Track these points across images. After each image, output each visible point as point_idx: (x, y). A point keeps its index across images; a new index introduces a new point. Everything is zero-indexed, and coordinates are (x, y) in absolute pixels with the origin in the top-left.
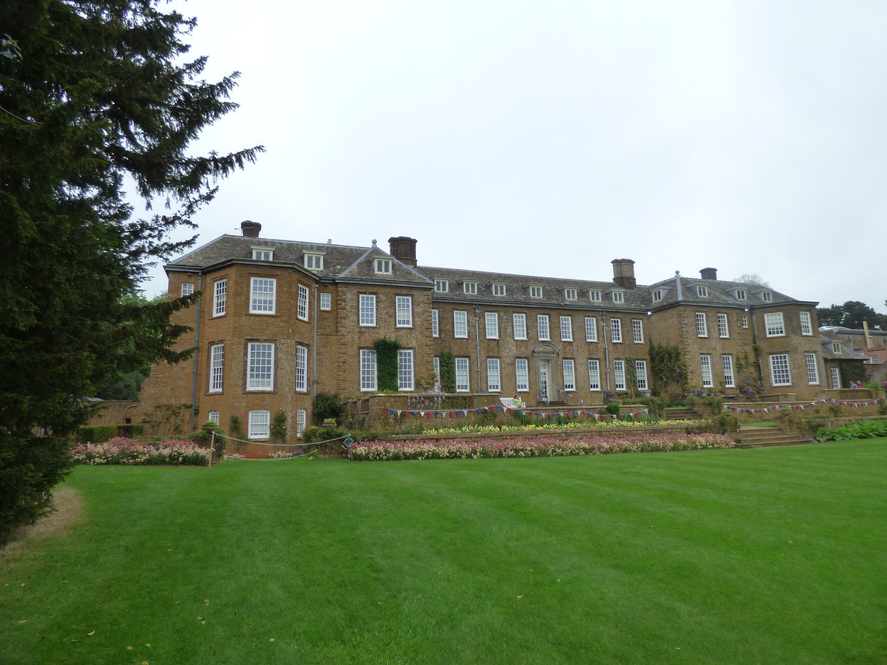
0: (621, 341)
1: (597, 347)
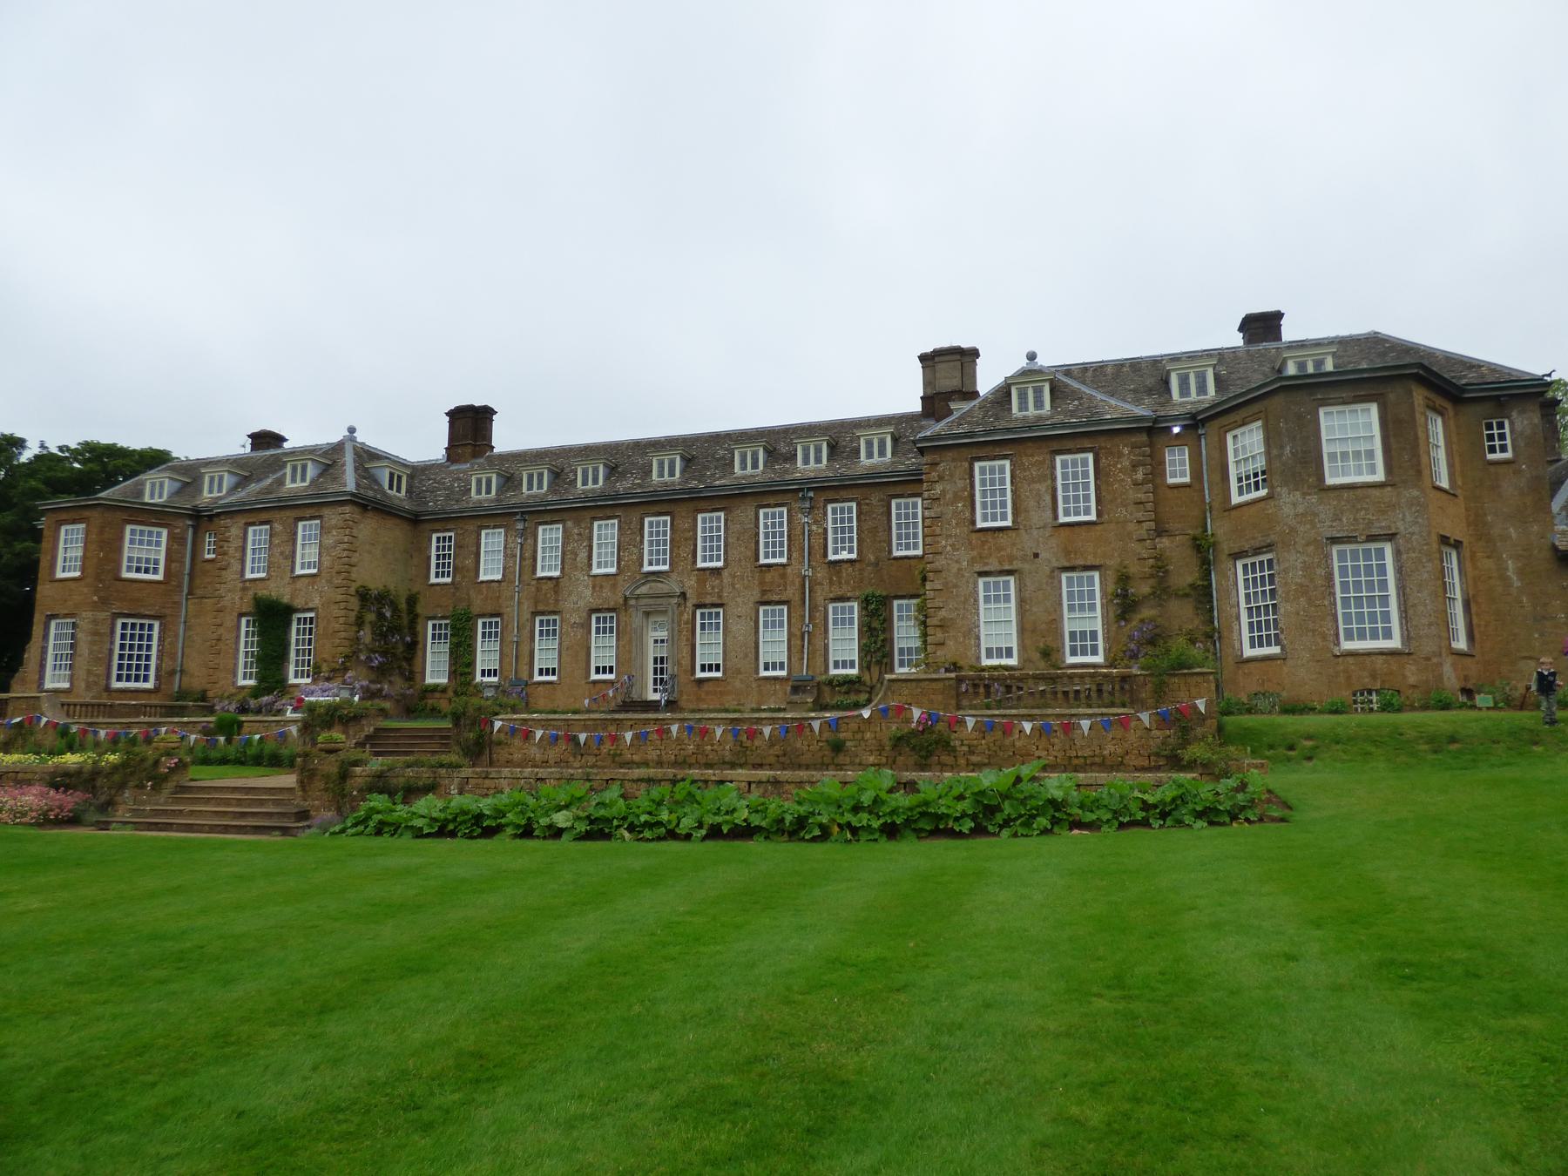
1: (783, 576)
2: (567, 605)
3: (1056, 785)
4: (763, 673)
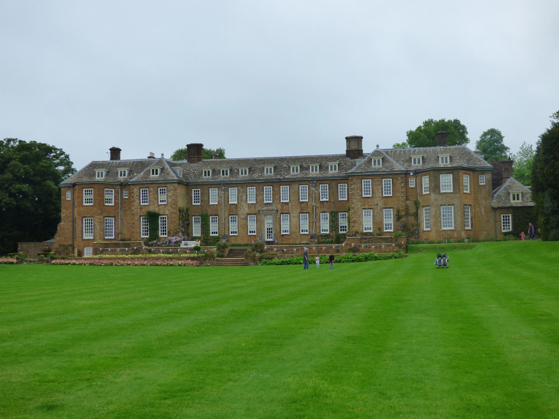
1: (307, 205)
3: (376, 255)
4: (301, 233)
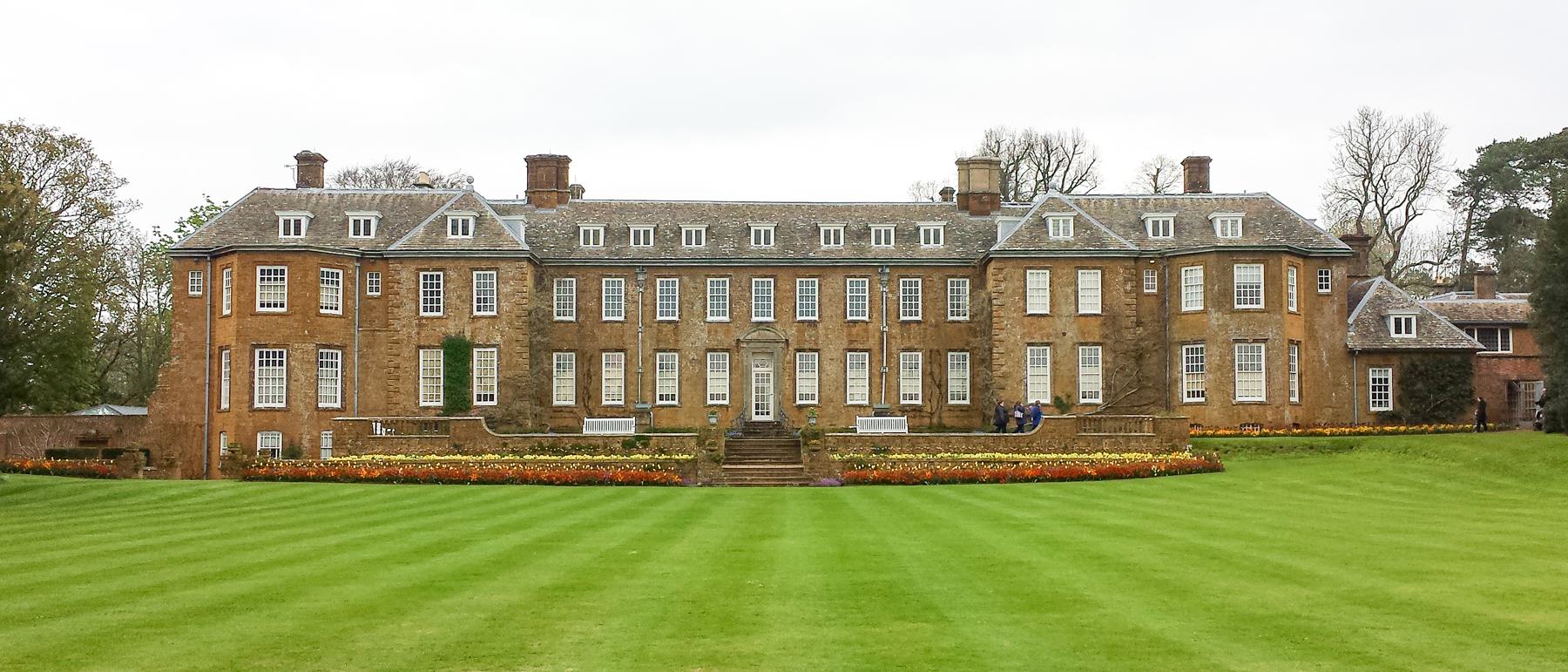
0: (919, 318)
1: (866, 330)
2: (685, 344)
